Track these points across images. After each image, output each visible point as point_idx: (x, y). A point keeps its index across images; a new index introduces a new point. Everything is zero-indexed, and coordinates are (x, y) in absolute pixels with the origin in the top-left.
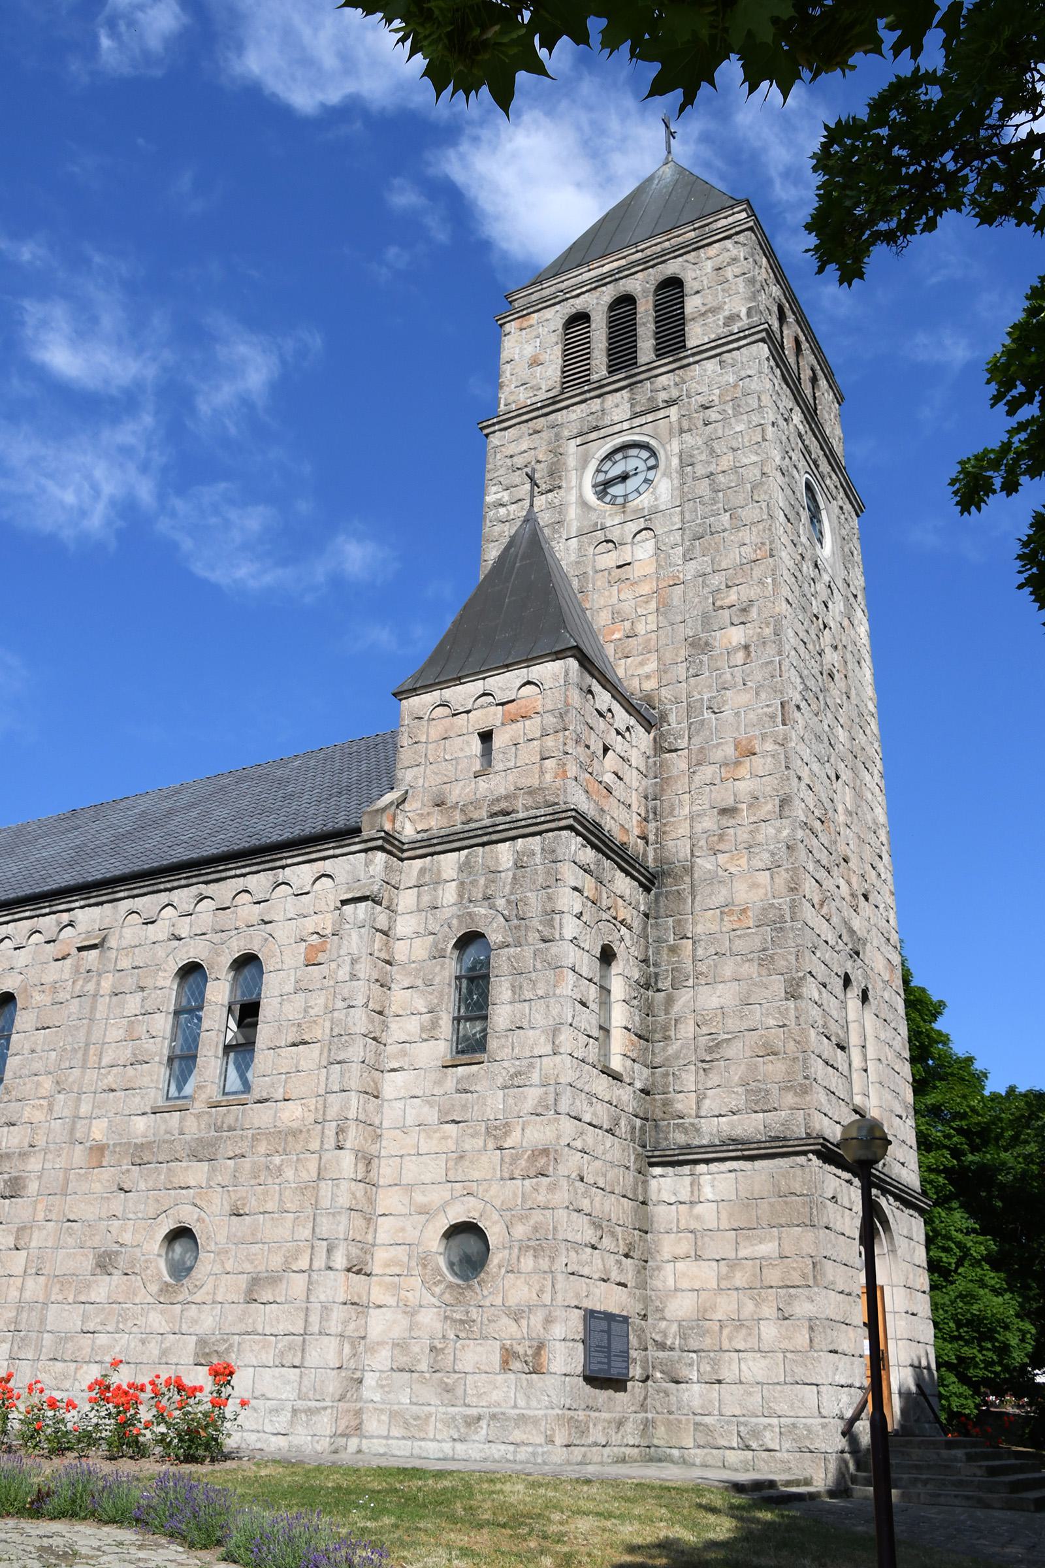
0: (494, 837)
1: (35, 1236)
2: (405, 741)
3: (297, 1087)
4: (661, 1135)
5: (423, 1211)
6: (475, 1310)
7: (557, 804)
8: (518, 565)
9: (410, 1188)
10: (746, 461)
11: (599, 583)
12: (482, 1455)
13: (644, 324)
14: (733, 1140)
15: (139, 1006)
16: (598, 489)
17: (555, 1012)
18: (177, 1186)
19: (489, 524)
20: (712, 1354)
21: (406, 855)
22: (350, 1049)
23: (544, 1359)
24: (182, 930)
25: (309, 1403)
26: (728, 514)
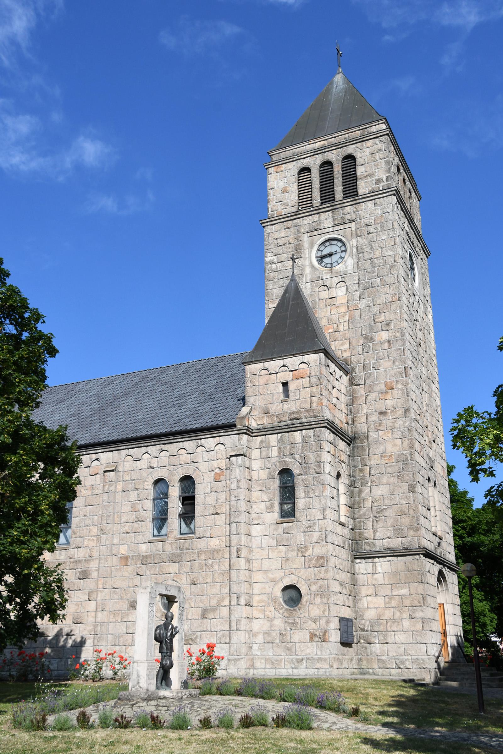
0: (293, 429)
1: (99, 595)
2: (248, 384)
3: (215, 532)
4: (359, 547)
5: (273, 581)
6: (297, 619)
7: (319, 416)
8: (291, 303)
9: (266, 572)
10: (387, 254)
11: (321, 305)
12: (305, 673)
13: (337, 178)
14: (389, 549)
15: (137, 497)
16: (318, 259)
17: (323, 502)
18: (165, 573)
19: (268, 272)
20: (384, 633)
21: (254, 434)
22: (240, 517)
23: (327, 637)
24: (154, 464)
25: (235, 657)
26: (379, 279)
